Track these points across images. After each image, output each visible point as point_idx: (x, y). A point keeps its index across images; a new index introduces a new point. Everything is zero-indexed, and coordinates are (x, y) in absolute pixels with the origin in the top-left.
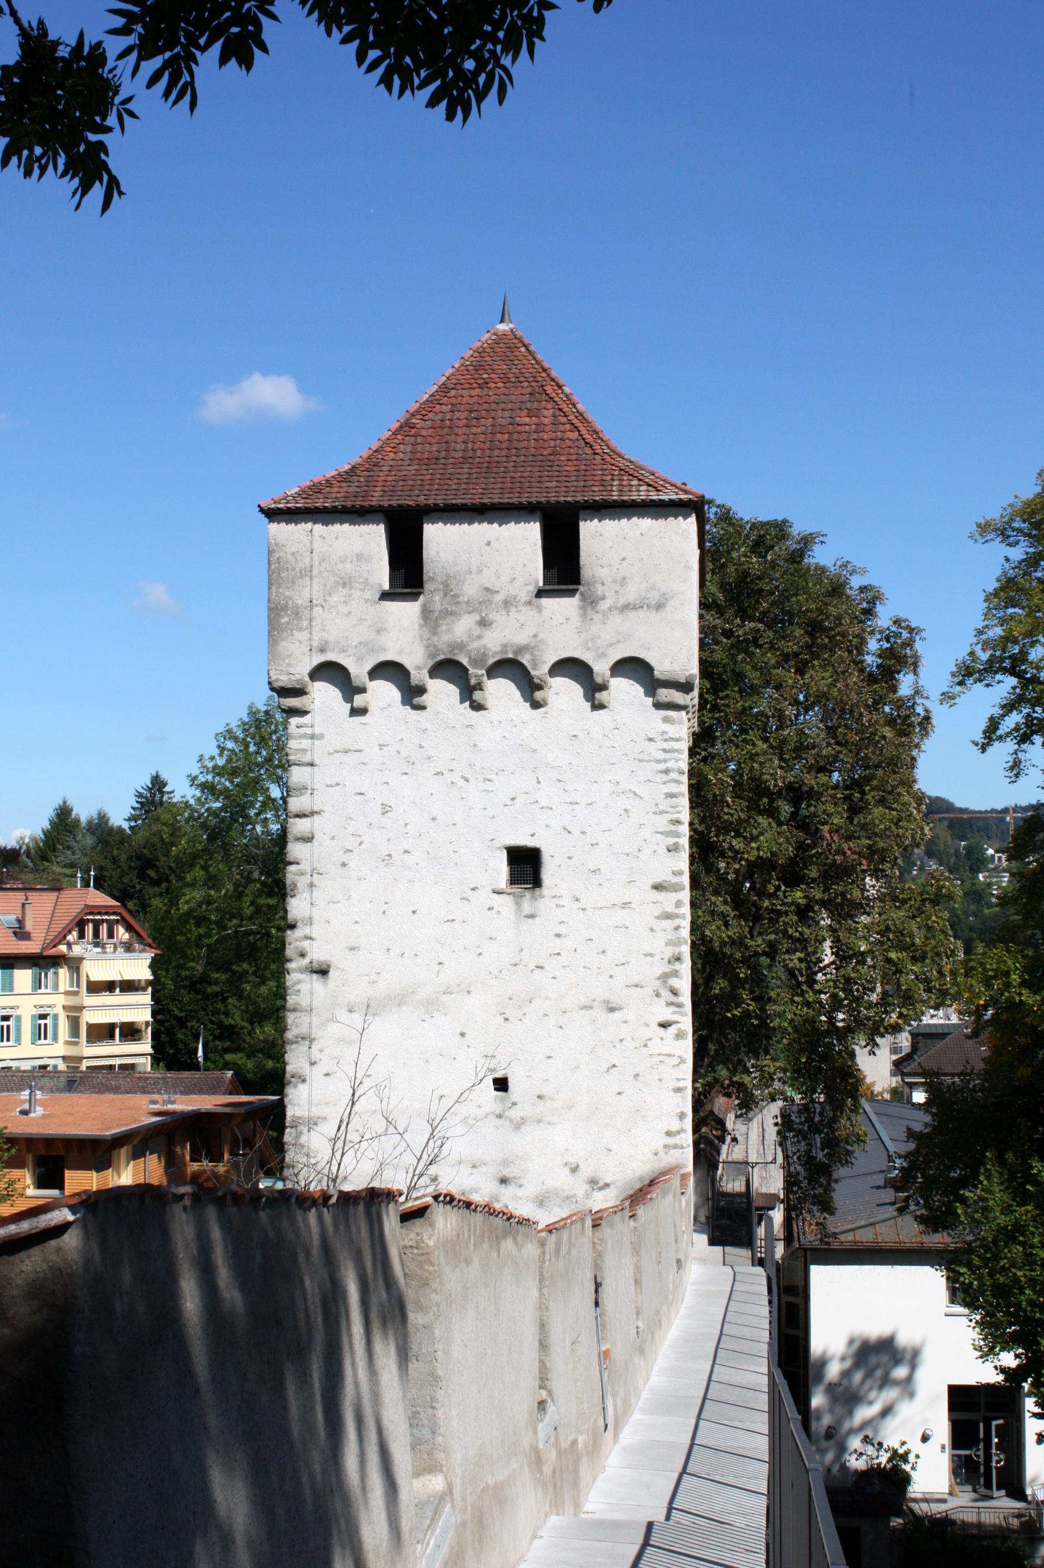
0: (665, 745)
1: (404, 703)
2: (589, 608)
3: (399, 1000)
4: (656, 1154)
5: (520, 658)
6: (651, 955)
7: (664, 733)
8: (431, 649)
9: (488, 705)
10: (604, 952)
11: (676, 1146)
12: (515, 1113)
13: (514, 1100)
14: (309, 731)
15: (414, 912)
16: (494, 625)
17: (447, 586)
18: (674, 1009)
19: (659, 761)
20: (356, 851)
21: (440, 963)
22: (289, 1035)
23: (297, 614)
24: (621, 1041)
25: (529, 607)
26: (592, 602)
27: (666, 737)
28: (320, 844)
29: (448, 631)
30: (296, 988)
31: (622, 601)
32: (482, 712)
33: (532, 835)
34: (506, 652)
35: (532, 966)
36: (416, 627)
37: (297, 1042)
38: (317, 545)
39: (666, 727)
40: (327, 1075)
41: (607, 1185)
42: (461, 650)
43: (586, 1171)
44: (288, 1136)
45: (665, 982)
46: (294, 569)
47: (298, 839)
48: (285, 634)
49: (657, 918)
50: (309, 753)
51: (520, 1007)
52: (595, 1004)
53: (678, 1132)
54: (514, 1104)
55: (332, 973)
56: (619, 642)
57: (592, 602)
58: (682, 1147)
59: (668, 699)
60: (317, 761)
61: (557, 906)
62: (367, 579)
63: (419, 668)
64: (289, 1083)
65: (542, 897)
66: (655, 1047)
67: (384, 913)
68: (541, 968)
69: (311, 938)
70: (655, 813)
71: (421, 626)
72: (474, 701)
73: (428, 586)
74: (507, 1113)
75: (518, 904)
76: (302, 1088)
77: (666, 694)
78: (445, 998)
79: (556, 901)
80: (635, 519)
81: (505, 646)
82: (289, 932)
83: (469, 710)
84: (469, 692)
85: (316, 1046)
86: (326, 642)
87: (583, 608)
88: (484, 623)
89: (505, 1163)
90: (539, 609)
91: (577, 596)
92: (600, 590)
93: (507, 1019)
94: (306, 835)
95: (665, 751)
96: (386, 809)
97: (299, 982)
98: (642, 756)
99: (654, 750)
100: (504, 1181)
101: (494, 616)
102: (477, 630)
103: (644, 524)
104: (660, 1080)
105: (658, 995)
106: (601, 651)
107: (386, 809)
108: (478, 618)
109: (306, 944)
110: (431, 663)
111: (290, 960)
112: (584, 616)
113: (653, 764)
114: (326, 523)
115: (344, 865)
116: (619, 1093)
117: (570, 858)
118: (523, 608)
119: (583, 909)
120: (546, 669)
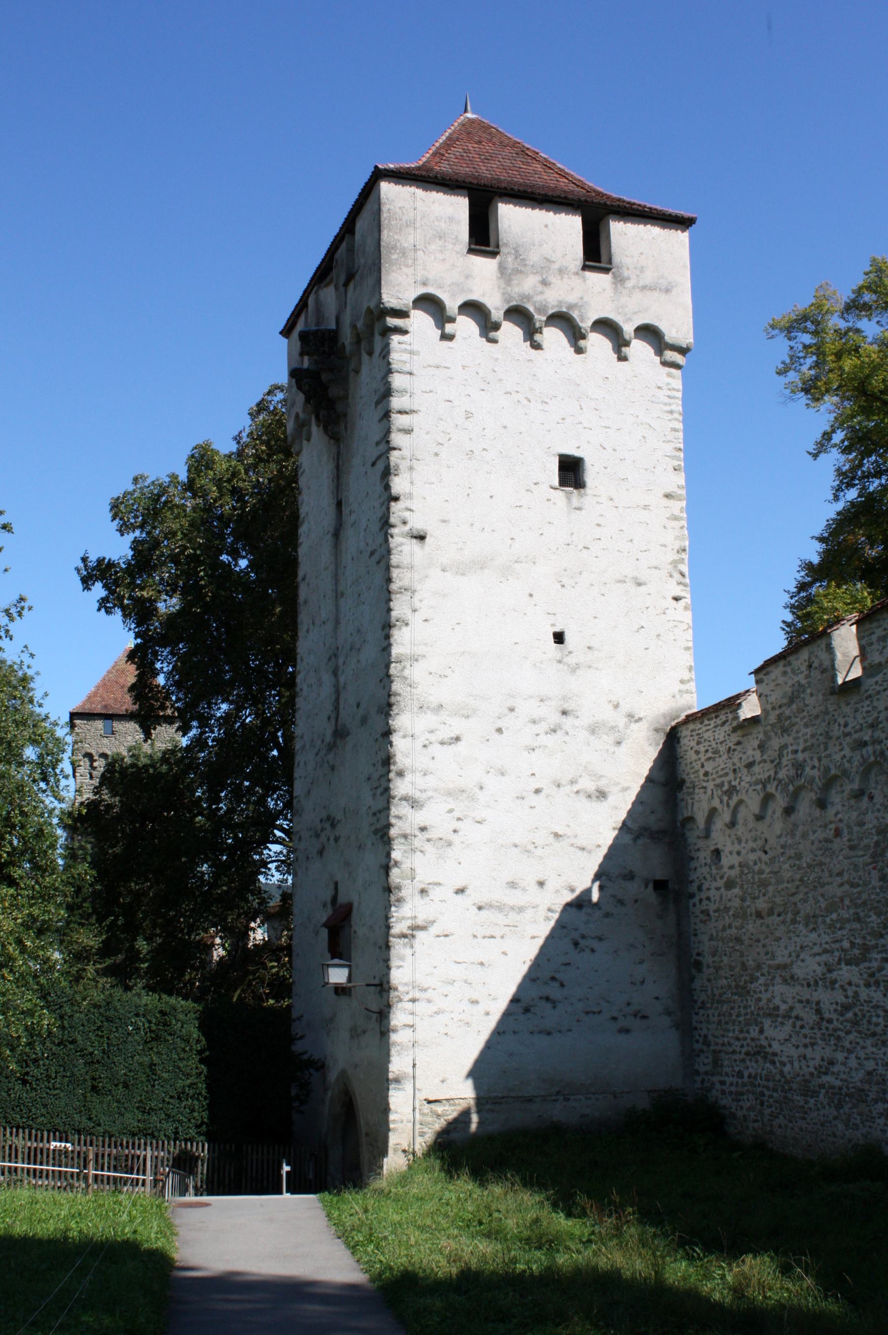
0: (669, 393)
1: (481, 335)
2: (619, 285)
3: (481, 564)
4: (674, 697)
5: (571, 313)
6: (665, 546)
7: (668, 384)
8: (507, 297)
9: (544, 346)
10: (631, 541)
11: (687, 692)
12: (571, 660)
13: (571, 649)
14: (408, 347)
15: (491, 497)
16: (552, 286)
17: (517, 251)
18: (681, 587)
19: (666, 404)
20: (446, 445)
21: (512, 539)
22: (394, 587)
23: (404, 253)
24: (647, 608)
25: (577, 277)
26: (621, 280)
27: (670, 387)
28: (418, 437)
29: (518, 284)
30: (399, 549)
31: (641, 283)
32: (540, 351)
33: (578, 448)
34: (561, 307)
35: (581, 547)
36: (495, 278)
37: (401, 593)
38: (419, 204)
39: (670, 380)
40: (426, 620)
41: (640, 719)
42: (528, 301)
43: (625, 708)
44: (394, 669)
45: (675, 567)
46: (401, 220)
47: (400, 430)
48: (394, 268)
49: (668, 518)
50: (408, 365)
51: (572, 577)
52: (627, 580)
53: (689, 681)
54: (570, 652)
55: (427, 540)
56: (640, 312)
57: (621, 280)
58: (692, 693)
59: (673, 359)
60: (415, 372)
61: (598, 502)
62: (457, 237)
63: (497, 309)
64: (395, 626)
65: (586, 494)
67: (468, 495)
68: (588, 548)
69: (411, 510)
70: (664, 441)
71: (498, 278)
72: (535, 341)
73: (503, 250)
74: (565, 660)
75: (569, 499)
76: (405, 629)
77: (671, 355)
78: (517, 566)
79: (597, 499)
80: (649, 226)
81: (561, 302)
82: (393, 504)
83: (530, 348)
84: (531, 332)
85: (417, 597)
86: (427, 279)
87: (615, 283)
88: (545, 283)
89: (565, 698)
90: (584, 279)
91: (610, 274)
92: (626, 273)
93: (563, 586)
94: (406, 428)
95: (669, 397)
96: (469, 415)
97: (401, 544)
98: (653, 399)
99: (662, 395)
100: (564, 713)
101: (551, 279)
102: (540, 288)
103: (653, 231)
104: (675, 640)
105: (671, 576)
106: (628, 316)
107: (469, 415)
108: (540, 279)
109: (407, 514)
110: (506, 307)
111: (393, 526)
112: (616, 289)
113: (661, 405)
114: (425, 189)
115: (436, 454)
116: (646, 649)
117: (605, 468)
118: (573, 277)
119: (616, 507)
120: (589, 323)
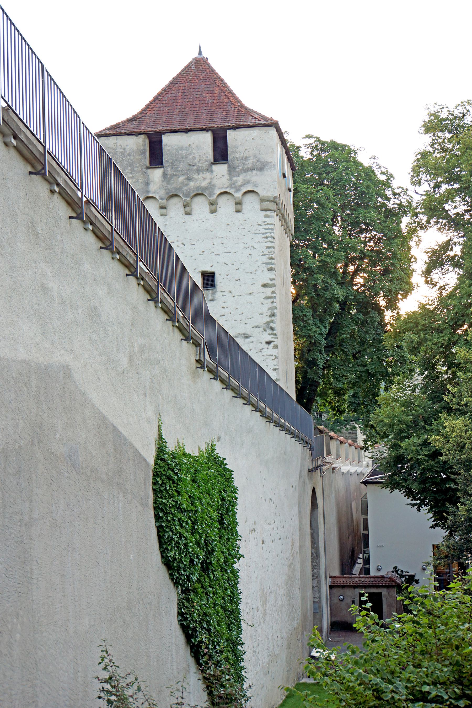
66: (265, 352)
